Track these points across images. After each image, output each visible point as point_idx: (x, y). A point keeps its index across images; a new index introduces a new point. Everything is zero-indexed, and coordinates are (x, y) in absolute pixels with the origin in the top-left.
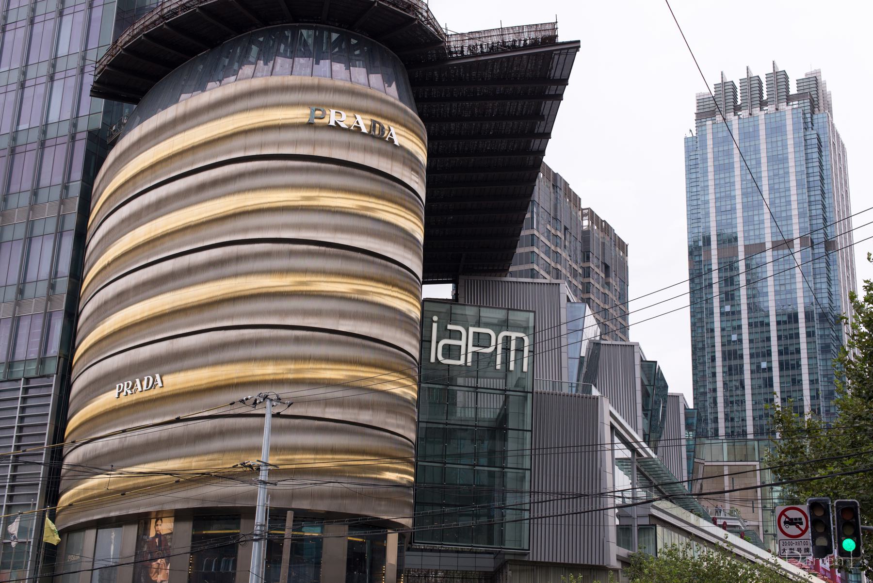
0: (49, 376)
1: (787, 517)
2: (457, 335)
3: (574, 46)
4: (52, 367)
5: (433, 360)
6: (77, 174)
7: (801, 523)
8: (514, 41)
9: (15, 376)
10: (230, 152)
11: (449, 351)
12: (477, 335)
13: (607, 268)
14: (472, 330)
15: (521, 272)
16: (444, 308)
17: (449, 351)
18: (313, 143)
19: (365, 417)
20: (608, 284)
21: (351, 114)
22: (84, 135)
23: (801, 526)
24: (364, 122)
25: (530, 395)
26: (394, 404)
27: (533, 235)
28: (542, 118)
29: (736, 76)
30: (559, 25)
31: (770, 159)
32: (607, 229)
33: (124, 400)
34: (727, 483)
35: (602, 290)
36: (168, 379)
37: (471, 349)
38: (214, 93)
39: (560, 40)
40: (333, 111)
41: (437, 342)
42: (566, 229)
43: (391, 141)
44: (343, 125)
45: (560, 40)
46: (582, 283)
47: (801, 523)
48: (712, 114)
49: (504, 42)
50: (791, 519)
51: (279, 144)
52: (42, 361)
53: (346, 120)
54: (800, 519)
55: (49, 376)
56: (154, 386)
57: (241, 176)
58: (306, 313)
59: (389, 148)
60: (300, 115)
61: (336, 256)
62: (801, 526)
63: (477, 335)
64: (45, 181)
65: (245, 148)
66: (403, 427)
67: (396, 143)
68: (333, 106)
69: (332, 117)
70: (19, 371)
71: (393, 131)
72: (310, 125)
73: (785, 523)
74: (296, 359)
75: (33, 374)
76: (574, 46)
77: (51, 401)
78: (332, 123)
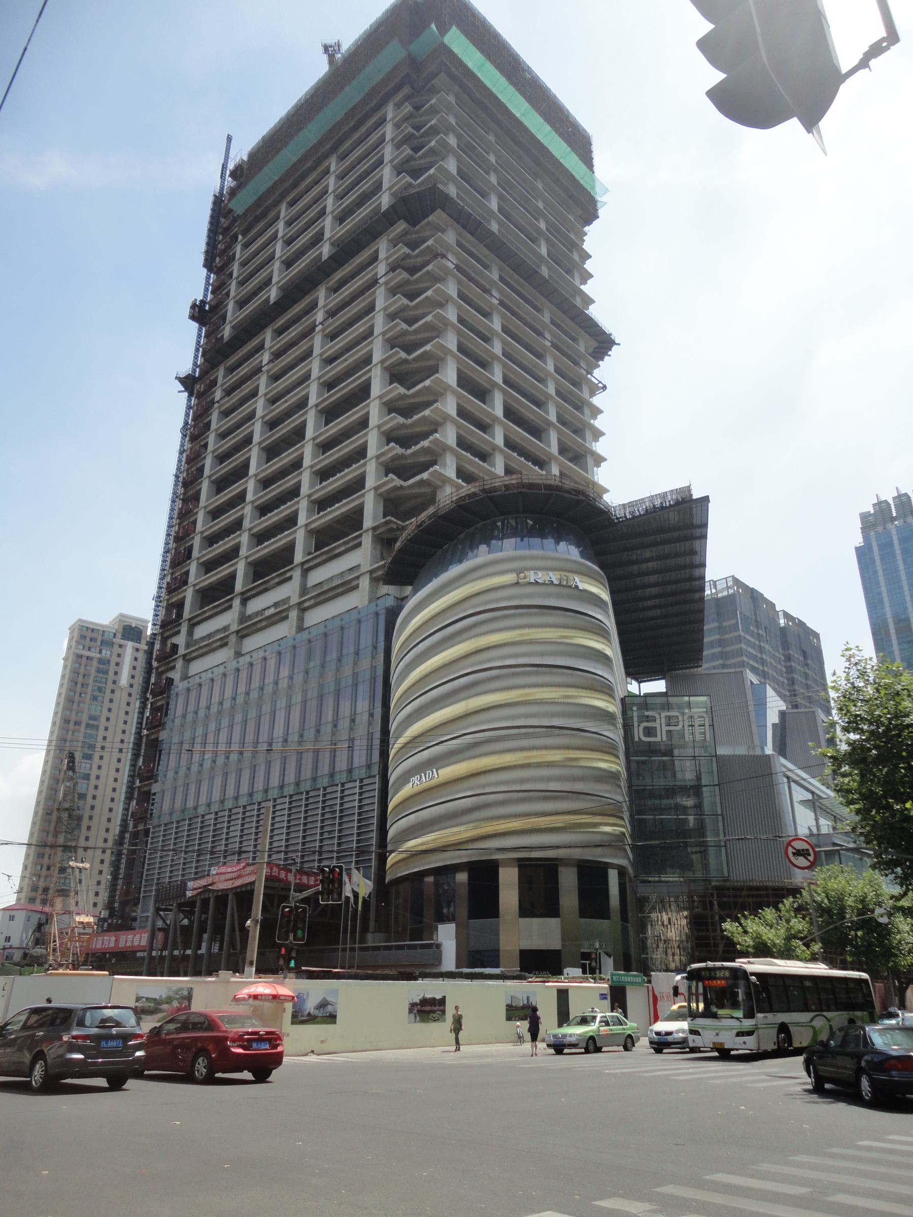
0: (374, 776)
1: (793, 848)
2: (653, 719)
3: (706, 499)
4: (375, 770)
5: (636, 739)
6: (381, 638)
7: (809, 855)
8: (662, 503)
9: (336, 782)
10: (466, 610)
11: (649, 732)
12: (669, 718)
13: (804, 654)
14: (663, 714)
15: (734, 664)
16: (663, 700)
17: (649, 732)
18: (521, 597)
19: (579, 787)
20: (807, 665)
21: (545, 573)
22: (384, 611)
23: (809, 858)
24: (554, 577)
25: (714, 759)
26: (612, 777)
27: (740, 636)
28: (695, 553)
29: (888, 496)
30: (692, 487)
31: (894, 556)
32: (801, 624)
33: (417, 789)
34: (335, 855)
35: (802, 670)
36: (441, 772)
37: (665, 728)
38: (455, 570)
39: (694, 497)
40: (532, 572)
41: (639, 726)
42: (766, 628)
43: (577, 587)
44: (539, 581)
45: (694, 497)
46: (786, 667)
47: (809, 855)
48: (874, 525)
49: (654, 506)
50: (798, 851)
51: (498, 600)
52: (369, 767)
53: (541, 577)
54: (807, 850)
55: (374, 776)
56: (433, 778)
57: (475, 625)
58: (527, 716)
59: (576, 592)
60: (510, 578)
61: (545, 673)
62: (809, 858)
63: (669, 718)
64: (362, 646)
65: (475, 606)
66: (609, 792)
67: (581, 588)
68: (529, 569)
69: (532, 577)
70: (356, 775)
71: (577, 579)
72: (517, 583)
73: (794, 854)
74: (522, 749)
75: (364, 776)
76: (706, 499)
77: (376, 793)
78: (532, 581)
